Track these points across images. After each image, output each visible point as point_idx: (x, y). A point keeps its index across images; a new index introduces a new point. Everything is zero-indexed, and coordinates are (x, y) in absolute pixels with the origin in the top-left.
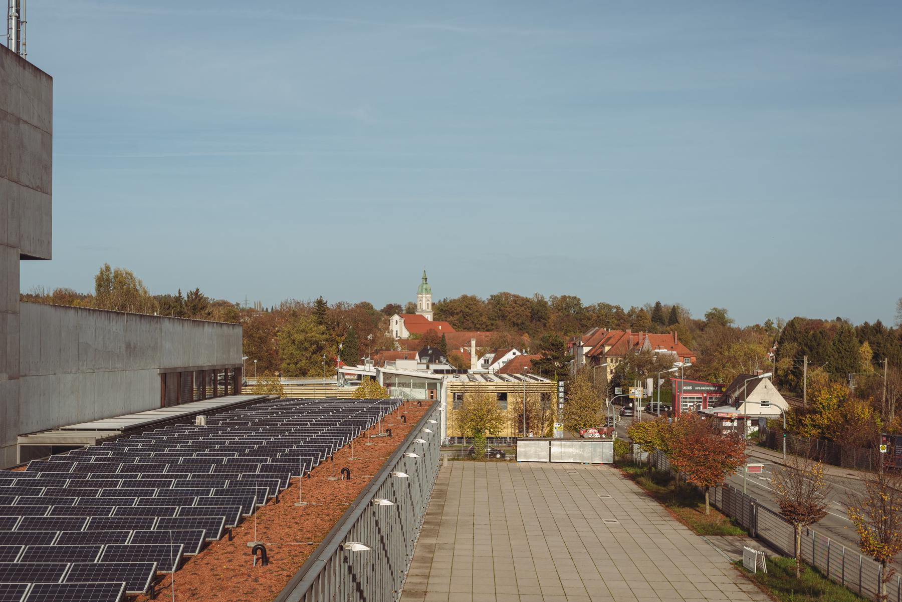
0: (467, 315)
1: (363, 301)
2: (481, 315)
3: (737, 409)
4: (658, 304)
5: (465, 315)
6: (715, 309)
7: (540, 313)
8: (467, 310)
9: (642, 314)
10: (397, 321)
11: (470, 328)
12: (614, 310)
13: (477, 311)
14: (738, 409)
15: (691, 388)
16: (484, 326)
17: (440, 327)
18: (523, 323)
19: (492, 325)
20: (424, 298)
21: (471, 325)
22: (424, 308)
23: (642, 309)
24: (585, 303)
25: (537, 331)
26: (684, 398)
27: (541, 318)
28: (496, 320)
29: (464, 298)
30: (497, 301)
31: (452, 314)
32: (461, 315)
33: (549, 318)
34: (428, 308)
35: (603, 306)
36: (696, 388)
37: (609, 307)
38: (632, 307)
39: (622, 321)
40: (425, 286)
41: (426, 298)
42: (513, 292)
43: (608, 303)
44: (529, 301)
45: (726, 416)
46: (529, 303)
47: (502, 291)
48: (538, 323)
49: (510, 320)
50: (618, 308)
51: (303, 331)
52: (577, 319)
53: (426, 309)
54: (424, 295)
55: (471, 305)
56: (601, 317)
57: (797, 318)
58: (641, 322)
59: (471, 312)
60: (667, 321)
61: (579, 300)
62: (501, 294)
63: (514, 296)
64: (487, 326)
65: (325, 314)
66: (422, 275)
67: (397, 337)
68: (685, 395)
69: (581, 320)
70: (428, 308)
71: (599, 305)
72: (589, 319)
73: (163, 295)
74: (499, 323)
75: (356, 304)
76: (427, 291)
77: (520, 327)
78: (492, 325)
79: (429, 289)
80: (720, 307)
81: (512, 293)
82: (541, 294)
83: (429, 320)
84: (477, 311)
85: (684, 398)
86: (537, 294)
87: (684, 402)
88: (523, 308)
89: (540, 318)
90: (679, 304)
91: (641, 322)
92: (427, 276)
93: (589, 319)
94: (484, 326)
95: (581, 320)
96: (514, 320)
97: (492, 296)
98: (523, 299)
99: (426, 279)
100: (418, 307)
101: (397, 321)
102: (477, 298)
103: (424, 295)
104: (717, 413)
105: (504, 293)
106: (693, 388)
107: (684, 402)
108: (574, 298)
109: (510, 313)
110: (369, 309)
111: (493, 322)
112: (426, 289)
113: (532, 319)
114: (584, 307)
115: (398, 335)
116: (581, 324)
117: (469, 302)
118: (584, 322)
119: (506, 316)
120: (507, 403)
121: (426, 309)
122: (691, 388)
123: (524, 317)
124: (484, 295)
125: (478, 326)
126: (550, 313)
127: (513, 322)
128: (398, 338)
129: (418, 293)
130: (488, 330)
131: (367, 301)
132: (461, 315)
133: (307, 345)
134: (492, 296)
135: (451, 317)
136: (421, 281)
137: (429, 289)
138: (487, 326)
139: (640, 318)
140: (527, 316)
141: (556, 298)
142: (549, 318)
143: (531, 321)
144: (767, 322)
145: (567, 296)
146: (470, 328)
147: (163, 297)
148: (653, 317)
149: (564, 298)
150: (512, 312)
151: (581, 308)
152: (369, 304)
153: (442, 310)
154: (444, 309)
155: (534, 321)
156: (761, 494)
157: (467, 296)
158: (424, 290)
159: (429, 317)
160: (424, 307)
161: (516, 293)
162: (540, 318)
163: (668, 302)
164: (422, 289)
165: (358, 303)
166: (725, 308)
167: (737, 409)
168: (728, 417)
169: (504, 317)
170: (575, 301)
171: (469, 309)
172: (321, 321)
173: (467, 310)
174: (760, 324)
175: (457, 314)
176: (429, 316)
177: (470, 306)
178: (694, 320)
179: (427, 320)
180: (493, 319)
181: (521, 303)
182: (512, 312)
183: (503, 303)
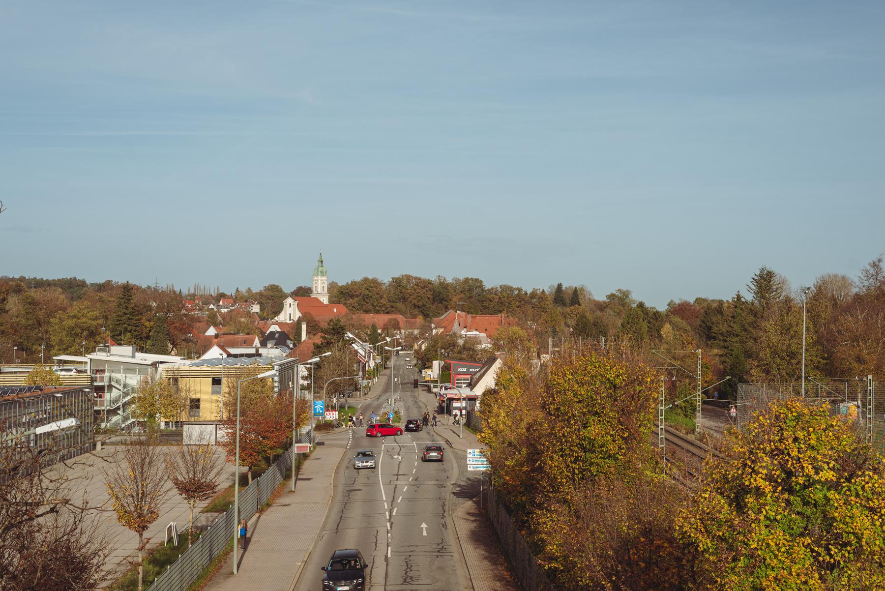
0: (367, 298)
1: (271, 283)
2: (381, 297)
3: (471, 390)
4: (560, 286)
5: (365, 298)
6: (620, 290)
7: (441, 295)
8: (367, 292)
9: (543, 296)
10: (290, 304)
11: (371, 310)
12: (516, 292)
13: (377, 293)
14: (473, 390)
15: (465, 370)
16: (384, 309)
17: (335, 310)
18: (424, 306)
19: (392, 307)
20: (319, 281)
21: (370, 307)
22: (319, 291)
23: (543, 291)
24: (488, 285)
25: (439, 313)
26: (458, 380)
27: (443, 299)
28: (396, 302)
29: (366, 280)
30: (398, 283)
31: (352, 297)
32: (360, 297)
33: (451, 300)
34: (323, 291)
35: (507, 289)
36: (459, 370)
37: (511, 289)
38: (534, 289)
39: (523, 302)
40: (320, 269)
41: (321, 280)
42: (415, 274)
43: (510, 284)
44: (431, 284)
45: (455, 397)
46: (431, 285)
47: (404, 274)
48: (440, 305)
49: (411, 302)
50: (520, 290)
51: (75, 317)
52: (479, 301)
53: (321, 292)
54: (320, 278)
55: (371, 287)
56: (503, 299)
57: (699, 298)
58: (542, 304)
59: (370, 294)
60: (568, 302)
61: (481, 282)
62: (403, 276)
63: (416, 278)
64: (386, 308)
65: (132, 299)
66: (318, 258)
67: (290, 320)
68: (460, 377)
69: (482, 302)
70: (323, 291)
71: (501, 287)
72: (491, 301)
73: (68, 278)
74: (400, 305)
75: (265, 287)
76: (323, 274)
77: (421, 309)
78: (392, 307)
79: (324, 272)
80: (624, 289)
81: (414, 275)
82: (443, 276)
83: (325, 303)
84: (377, 293)
85: (458, 380)
86: (439, 276)
87: (458, 383)
88: (424, 290)
89: (442, 300)
90: (583, 285)
91: (542, 304)
92: (323, 259)
93: (491, 301)
94: (384, 309)
95: (482, 302)
96: (415, 302)
97: (393, 278)
98: (424, 281)
99: (322, 261)
100: (314, 290)
101: (290, 304)
102: (379, 281)
103: (320, 278)
104: (446, 394)
105: (406, 275)
106: (468, 370)
107: (458, 383)
108: (477, 280)
109: (411, 295)
110: (277, 291)
111: (393, 304)
112: (321, 272)
113: (434, 301)
114: (486, 289)
115: (292, 318)
116: (483, 306)
117: (371, 285)
118: (485, 304)
119: (408, 298)
120: (221, 388)
121: (321, 292)
122: (465, 370)
123: (426, 299)
124: (385, 278)
125: (377, 308)
126: (452, 295)
127: (414, 304)
128: (291, 321)
129: (314, 276)
130: (388, 313)
131: (276, 284)
132: (360, 297)
133: (79, 331)
134: (393, 278)
135: (351, 300)
136: (317, 264)
137: (324, 272)
138: (386, 308)
139: (541, 300)
140: (429, 298)
141: (459, 280)
142: (451, 300)
143: (433, 303)
144: (670, 303)
145: (470, 278)
146: (371, 310)
147: (67, 280)
148: (555, 299)
149: (467, 280)
150: (414, 294)
151: (483, 290)
152: (278, 286)
153: (342, 292)
154: (344, 292)
155: (436, 303)
156: (679, 444)
157: (368, 279)
158: (320, 273)
159: (325, 300)
160: (320, 290)
161: (418, 276)
162: (442, 300)
163: (568, 283)
164: (318, 272)
165: (267, 285)
166: (629, 289)
167: (471, 390)
168: (457, 397)
169: (404, 299)
170: (478, 283)
171: (370, 291)
172: (126, 306)
173: (367, 292)
174: (332, 318)
175: (357, 296)
176: (325, 299)
177: (370, 289)
178: (595, 301)
179: (323, 303)
180: (393, 302)
181: (422, 285)
182: (414, 294)
183: (404, 285)
